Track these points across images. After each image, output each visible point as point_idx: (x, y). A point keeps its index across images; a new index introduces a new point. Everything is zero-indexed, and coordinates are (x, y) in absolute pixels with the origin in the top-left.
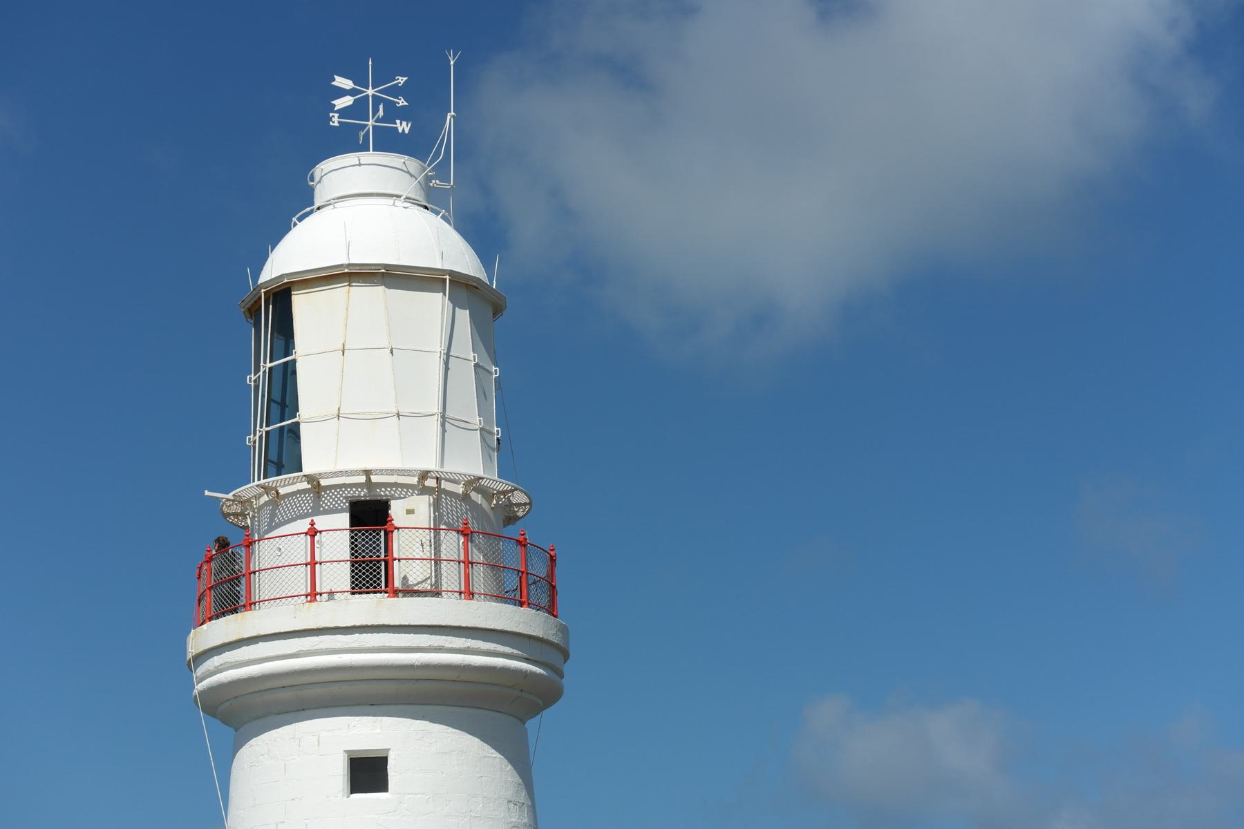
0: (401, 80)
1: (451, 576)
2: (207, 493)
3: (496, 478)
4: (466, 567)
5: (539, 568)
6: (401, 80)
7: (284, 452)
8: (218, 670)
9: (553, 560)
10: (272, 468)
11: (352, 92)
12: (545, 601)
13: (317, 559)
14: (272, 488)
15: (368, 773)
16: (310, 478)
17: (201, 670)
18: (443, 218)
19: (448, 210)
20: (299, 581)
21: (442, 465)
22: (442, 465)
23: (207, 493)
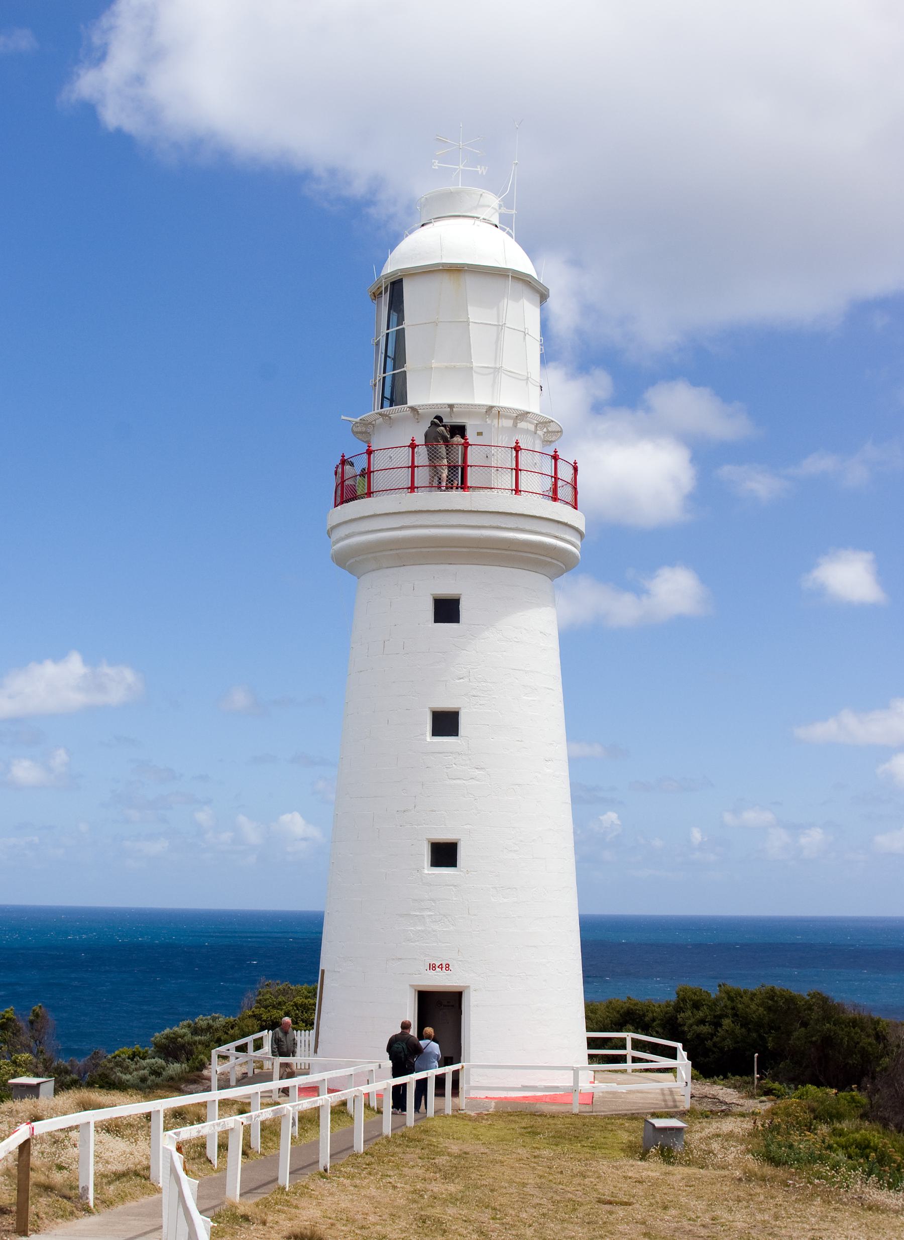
1: (423, 476)
2: (343, 417)
3: (313, 1032)
4: (517, 452)
5: (565, 473)
7: (395, 393)
8: (348, 536)
9: (576, 469)
10: (387, 403)
12: (570, 498)
13: (416, 464)
14: (386, 416)
15: (447, 610)
16: (413, 409)
17: (336, 535)
18: (508, 233)
19: (512, 229)
20: (403, 477)
21: (495, 363)
22: (495, 363)
23: (343, 417)
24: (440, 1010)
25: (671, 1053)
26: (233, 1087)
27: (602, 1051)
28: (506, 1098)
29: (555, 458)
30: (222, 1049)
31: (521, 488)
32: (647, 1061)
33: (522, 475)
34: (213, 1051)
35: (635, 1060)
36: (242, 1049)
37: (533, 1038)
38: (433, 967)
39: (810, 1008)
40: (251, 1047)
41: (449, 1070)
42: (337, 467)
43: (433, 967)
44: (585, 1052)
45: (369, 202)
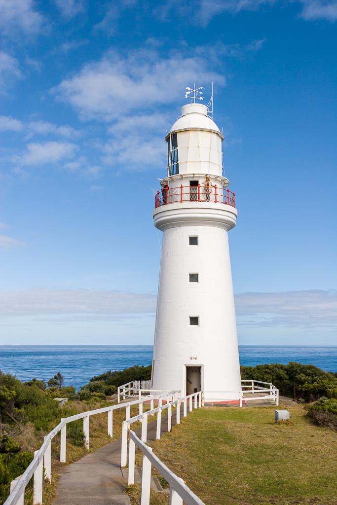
7: (176, 170)
9: (234, 195)
11: (190, 91)
13: (183, 193)
24: (194, 373)
25: (268, 387)
26: (119, 404)
27: (245, 387)
28: (195, 493)
29: (228, 191)
30: (121, 387)
31: (217, 200)
32: (259, 389)
33: (217, 196)
34: (118, 388)
35: (255, 389)
36: (127, 387)
37: (223, 385)
38: (191, 358)
39: (53, 26)
40: (129, 386)
41: (196, 395)
42: (156, 196)
43: (191, 358)
44: (241, 386)
45: (306, 419)
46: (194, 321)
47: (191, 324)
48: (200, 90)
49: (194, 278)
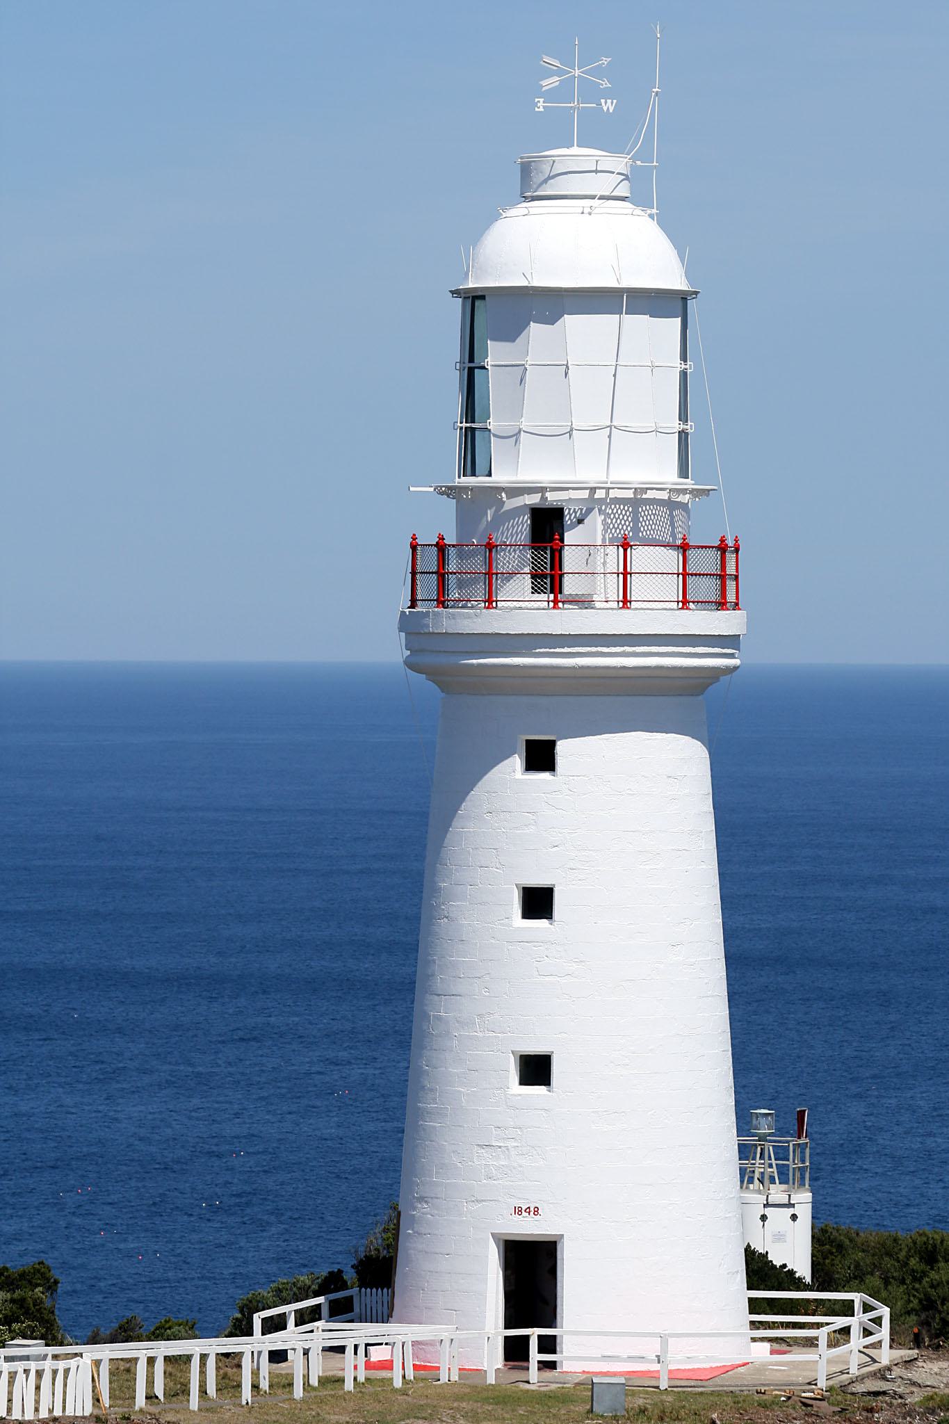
0: (605, 61)
6: (605, 61)
11: (560, 72)
38: (518, 1211)
43: (518, 1211)
46: (538, 902)
47: (524, 1082)
48: (598, 72)
49: (538, 902)
